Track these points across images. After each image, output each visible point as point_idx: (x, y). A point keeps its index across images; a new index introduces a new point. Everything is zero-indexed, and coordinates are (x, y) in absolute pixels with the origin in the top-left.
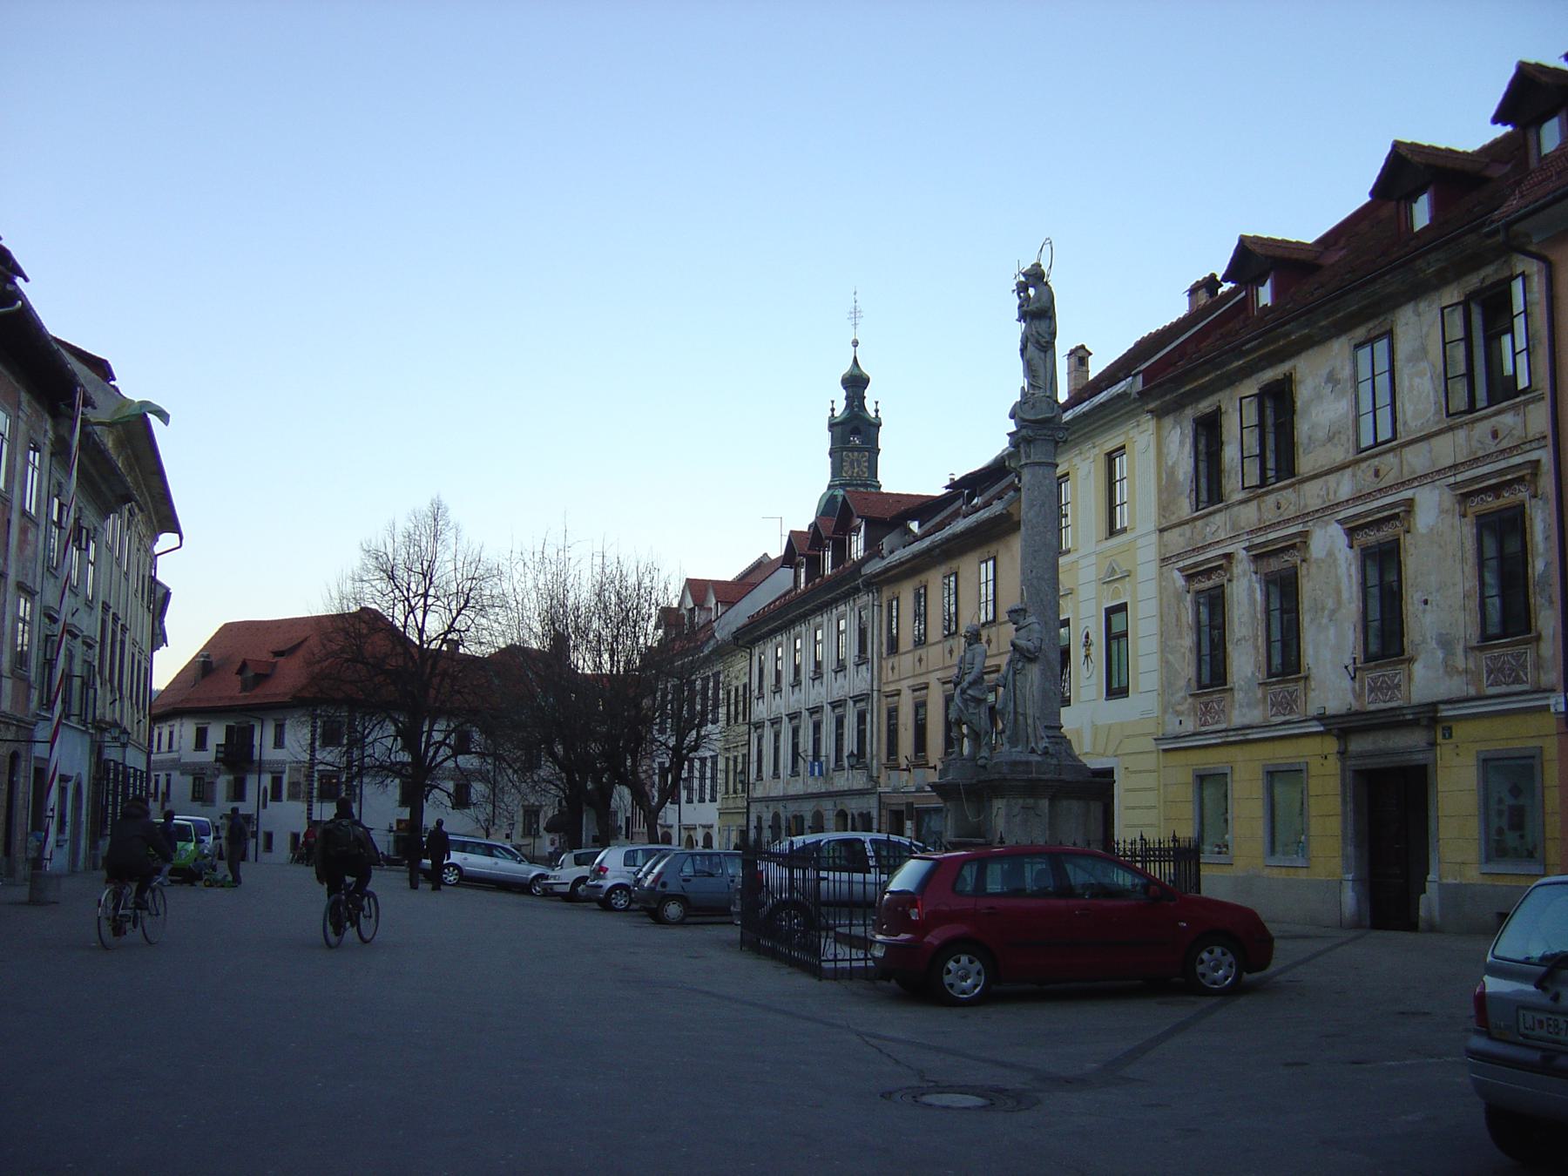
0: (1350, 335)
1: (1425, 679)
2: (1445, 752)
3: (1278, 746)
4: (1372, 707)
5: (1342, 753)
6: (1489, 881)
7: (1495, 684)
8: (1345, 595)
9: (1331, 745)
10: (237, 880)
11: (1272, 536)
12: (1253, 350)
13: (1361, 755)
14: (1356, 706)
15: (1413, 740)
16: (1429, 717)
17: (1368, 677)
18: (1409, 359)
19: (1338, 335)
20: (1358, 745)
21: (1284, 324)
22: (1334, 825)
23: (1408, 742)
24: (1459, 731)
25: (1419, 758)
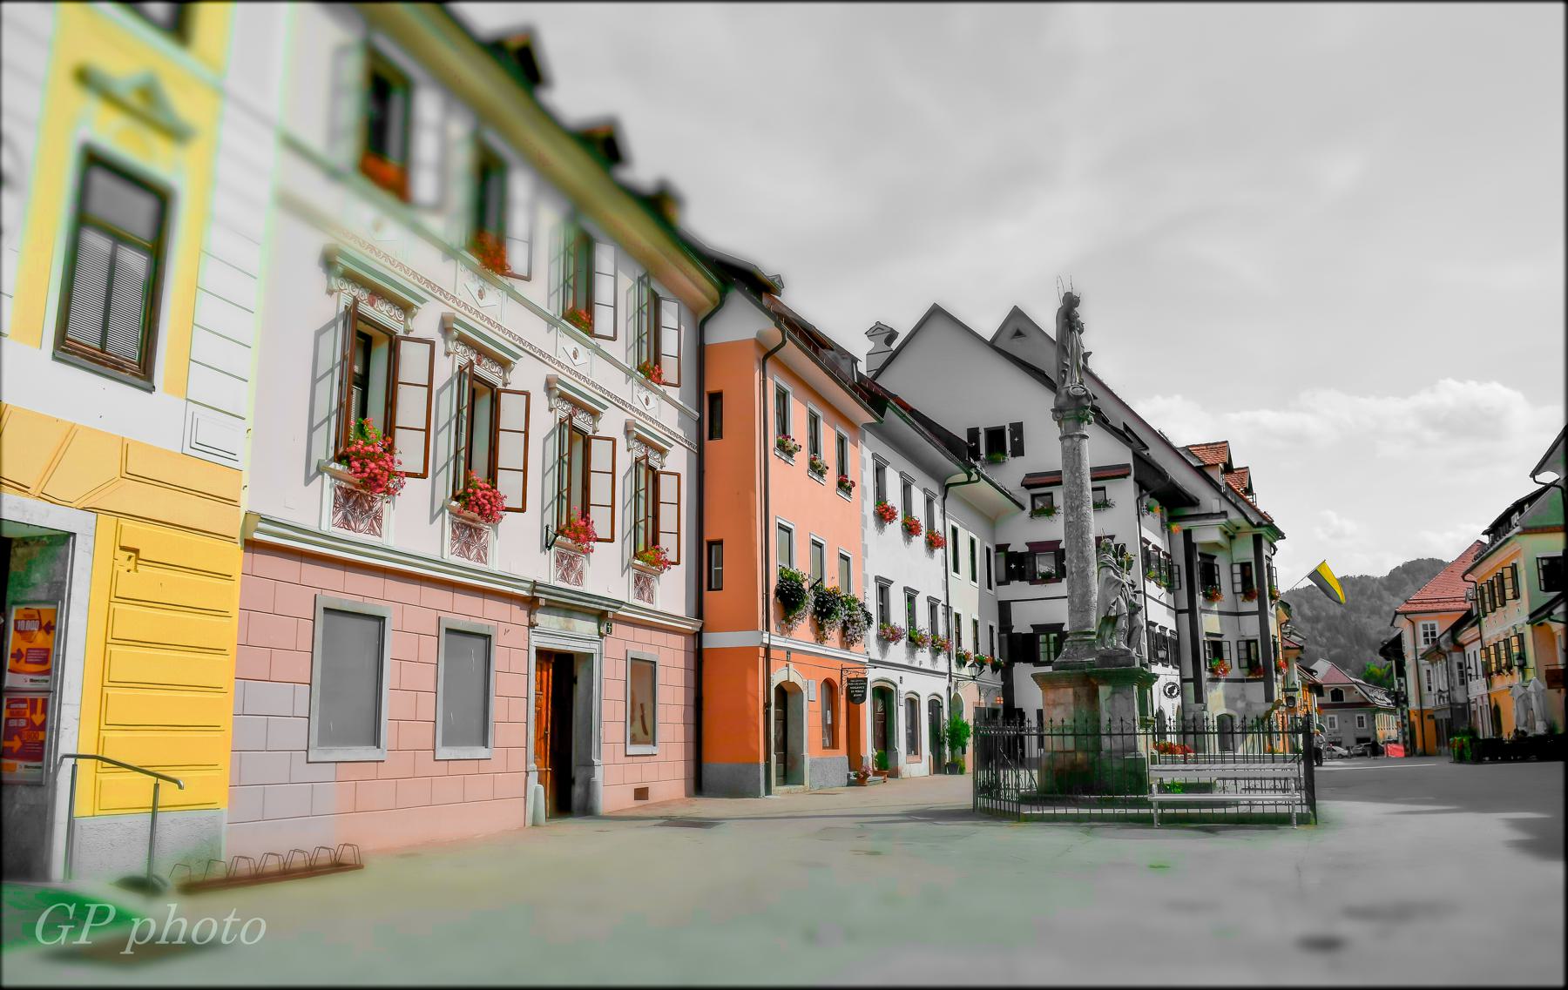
1: (605, 572)
15: (587, 627)
16: (602, 614)
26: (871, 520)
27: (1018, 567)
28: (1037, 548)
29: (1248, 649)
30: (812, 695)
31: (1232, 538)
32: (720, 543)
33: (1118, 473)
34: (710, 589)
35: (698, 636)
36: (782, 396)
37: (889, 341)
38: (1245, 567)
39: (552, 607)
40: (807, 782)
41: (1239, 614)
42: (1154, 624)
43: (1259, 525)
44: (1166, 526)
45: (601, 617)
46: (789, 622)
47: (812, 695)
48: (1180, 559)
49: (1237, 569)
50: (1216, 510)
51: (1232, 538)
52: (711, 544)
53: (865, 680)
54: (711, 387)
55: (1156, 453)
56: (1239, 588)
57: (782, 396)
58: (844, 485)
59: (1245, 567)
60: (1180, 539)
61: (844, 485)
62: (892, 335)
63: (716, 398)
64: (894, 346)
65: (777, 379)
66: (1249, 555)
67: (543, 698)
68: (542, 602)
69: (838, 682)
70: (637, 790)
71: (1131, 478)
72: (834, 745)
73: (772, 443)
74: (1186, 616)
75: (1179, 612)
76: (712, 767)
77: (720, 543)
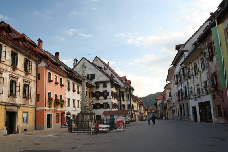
0: (26, 57)
1: (18, 100)
2: (19, 110)
3: (25, 108)
4: (10, 102)
5: (5, 108)
6: (23, 126)
7: (25, 103)
8: (8, 85)
9: (3, 107)
10: (222, 90)
11: (15, 75)
12: (2, 38)
13: (8, 109)
14: (8, 102)
15: (15, 108)
16: (18, 106)
17: (10, 98)
18: (19, 60)
19: (25, 56)
20: (7, 107)
21: (10, 41)
22: (192, 116)
23: (14, 108)
24: (21, 108)
25: (16, 111)
26: (67, 90)
27: (101, 94)
28: (104, 91)
29: (128, 106)
30: (54, 115)
31: (126, 90)
32: (39, 95)
33: (108, 82)
34: (38, 101)
35: (36, 108)
36: (50, 74)
37: (77, 61)
38: (128, 94)
39: (8, 105)
40: (53, 127)
41: (127, 101)
42: (113, 103)
43: (130, 88)
44: (116, 89)
45: (18, 106)
46: (106, 116)
47: (54, 115)
48: (118, 93)
49: (127, 94)
50: (124, 86)
51: (126, 90)
52: (38, 95)
53: (65, 113)
54: (38, 73)
55: (115, 78)
56: (127, 97)
57: (50, 74)
58: (62, 86)
59: (128, 94)
60: (119, 90)
61: (62, 86)
62: (77, 61)
63: (39, 74)
64: (78, 62)
65: (49, 71)
66: (129, 92)
67: (29, 39)
68: (7, 105)
69: (59, 113)
70: (24, 130)
71: (110, 82)
72: (58, 122)
73: (47, 80)
74: (119, 101)
75: (118, 101)
76: (37, 128)
77: (39, 95)
